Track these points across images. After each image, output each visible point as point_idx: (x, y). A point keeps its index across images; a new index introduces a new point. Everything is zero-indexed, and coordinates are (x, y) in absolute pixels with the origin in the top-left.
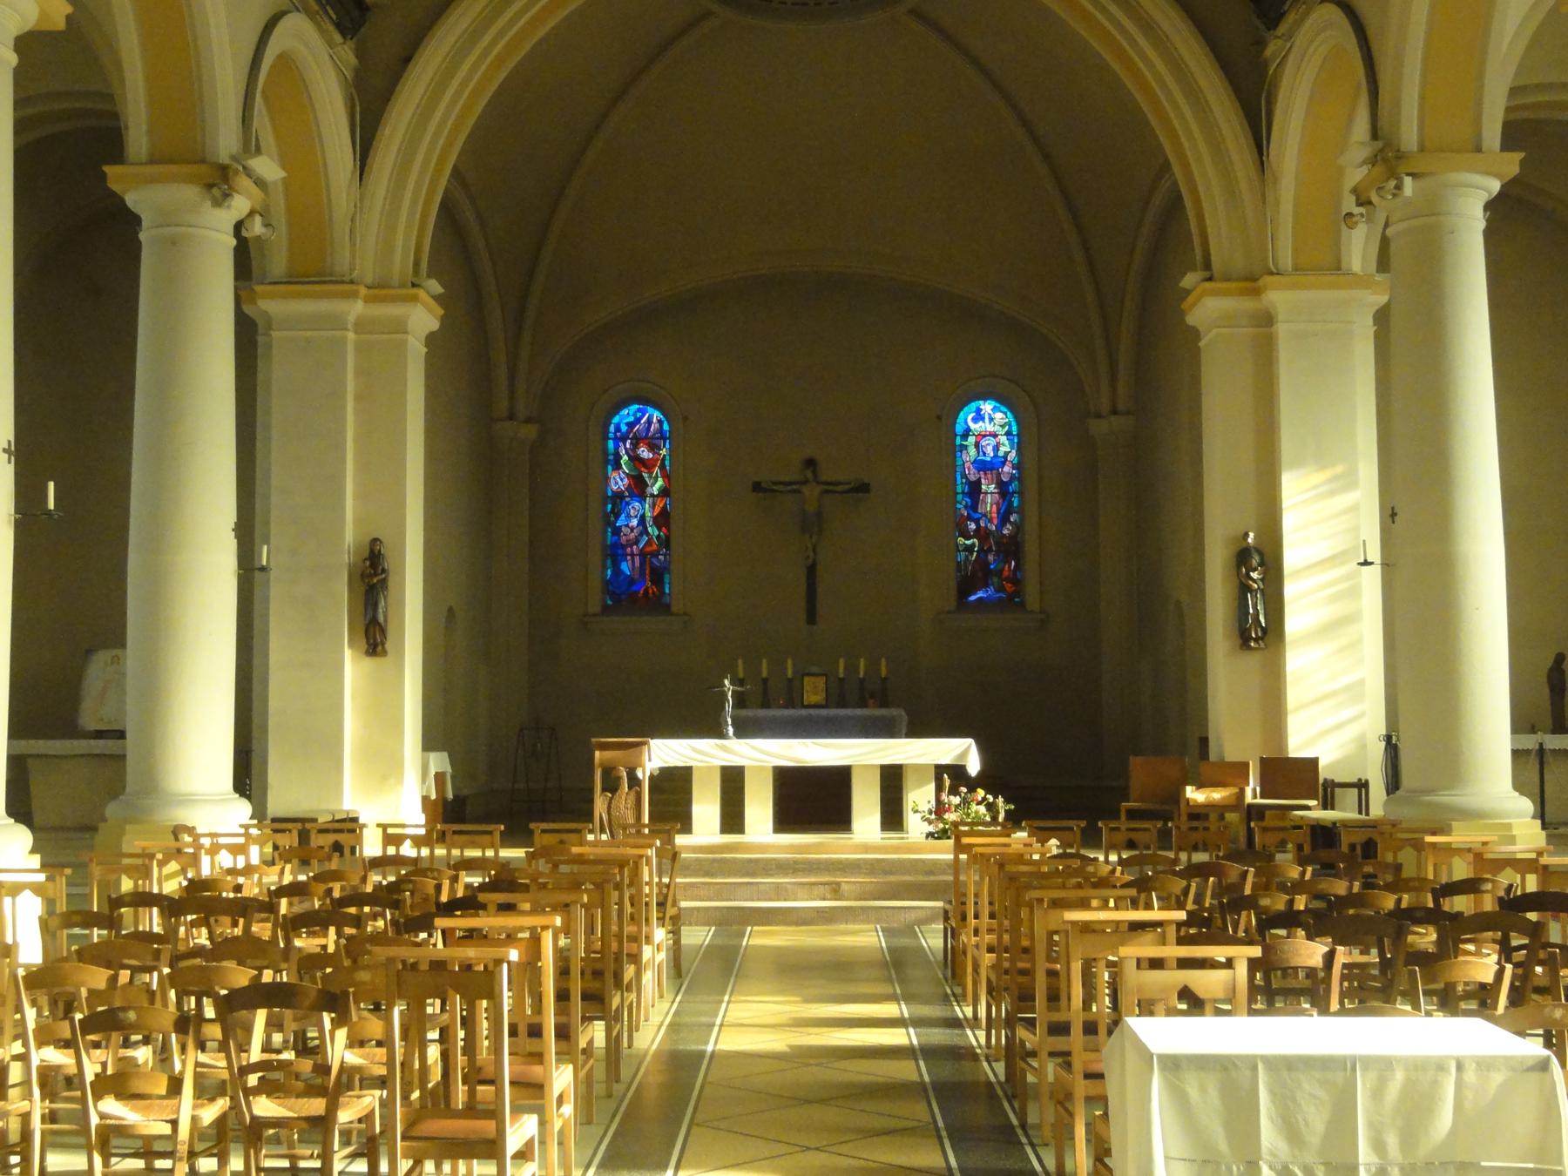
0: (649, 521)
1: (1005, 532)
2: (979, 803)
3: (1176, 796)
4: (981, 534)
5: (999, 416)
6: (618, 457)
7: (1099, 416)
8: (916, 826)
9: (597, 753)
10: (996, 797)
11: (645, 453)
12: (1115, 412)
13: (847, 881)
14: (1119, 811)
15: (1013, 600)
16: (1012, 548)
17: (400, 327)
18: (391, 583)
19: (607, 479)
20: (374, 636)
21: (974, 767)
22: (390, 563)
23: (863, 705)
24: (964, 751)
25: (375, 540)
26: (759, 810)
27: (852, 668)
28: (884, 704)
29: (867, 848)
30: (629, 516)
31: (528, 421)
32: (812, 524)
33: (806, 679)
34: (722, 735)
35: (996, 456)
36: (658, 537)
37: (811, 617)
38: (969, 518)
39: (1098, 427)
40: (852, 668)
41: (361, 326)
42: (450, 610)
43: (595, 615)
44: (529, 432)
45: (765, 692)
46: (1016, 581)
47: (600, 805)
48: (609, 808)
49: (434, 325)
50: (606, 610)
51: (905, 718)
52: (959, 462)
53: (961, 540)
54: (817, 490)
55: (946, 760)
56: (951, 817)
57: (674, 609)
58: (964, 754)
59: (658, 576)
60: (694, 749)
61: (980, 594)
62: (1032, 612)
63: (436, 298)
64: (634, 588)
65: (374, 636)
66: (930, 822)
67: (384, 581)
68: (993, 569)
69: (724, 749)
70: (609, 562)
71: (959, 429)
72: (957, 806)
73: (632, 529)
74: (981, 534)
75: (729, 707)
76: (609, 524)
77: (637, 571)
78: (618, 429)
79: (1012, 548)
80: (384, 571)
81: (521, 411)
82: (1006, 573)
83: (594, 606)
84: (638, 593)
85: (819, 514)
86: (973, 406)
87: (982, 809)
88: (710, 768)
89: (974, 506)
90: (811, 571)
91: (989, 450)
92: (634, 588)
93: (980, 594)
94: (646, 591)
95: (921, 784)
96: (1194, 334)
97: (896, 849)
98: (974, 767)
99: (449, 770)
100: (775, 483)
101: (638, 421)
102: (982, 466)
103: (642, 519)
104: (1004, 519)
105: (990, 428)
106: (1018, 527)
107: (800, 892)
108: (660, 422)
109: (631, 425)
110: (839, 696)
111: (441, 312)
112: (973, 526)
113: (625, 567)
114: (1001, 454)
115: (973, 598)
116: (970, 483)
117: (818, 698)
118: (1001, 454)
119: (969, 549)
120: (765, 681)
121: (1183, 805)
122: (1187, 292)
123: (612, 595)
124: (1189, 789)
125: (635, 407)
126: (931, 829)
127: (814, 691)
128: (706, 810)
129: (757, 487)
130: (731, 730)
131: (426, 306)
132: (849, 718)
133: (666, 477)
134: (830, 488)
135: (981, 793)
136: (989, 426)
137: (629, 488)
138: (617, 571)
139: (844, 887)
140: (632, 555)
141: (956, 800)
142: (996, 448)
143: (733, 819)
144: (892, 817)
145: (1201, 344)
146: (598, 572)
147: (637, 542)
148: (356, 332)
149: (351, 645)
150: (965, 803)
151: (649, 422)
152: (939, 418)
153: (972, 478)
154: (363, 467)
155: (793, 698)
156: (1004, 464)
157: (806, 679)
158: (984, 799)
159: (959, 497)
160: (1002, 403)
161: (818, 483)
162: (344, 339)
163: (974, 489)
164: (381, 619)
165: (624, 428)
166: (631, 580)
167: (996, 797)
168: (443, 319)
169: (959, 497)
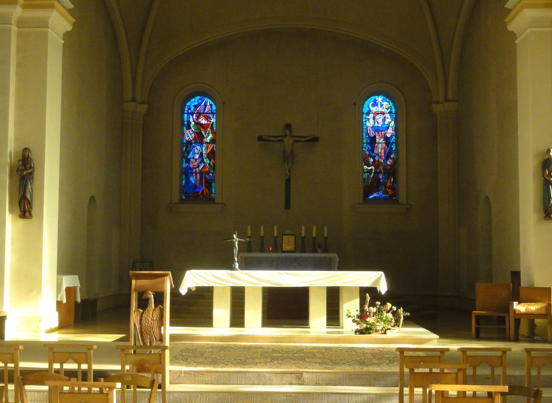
0: (205, 155)
1: (388, 163)
2: (388, 312)
3: (507, 308)
4: (376, 164)
5: (385, 103)
6: (189, 123)
7: (438, 102)
8: (348, 325)
9: (134, 282)
10: (398, 308)
11: (203, 121)
12: (446, 100)
13: (309, 370)
14: (470, 314)
15: (392, 198)
16: (392, 172)
17: (44, 24)
18: (36, 175)
19: (183, 134)
20: (25, 207)
21: (383, 288)
22: (36, 164)
23: (315, 251)
24: (377, 279)
25: (26, 149)
26: (254, 312)
27: (309, 231)
28: (325, 251)
29: (318, 339)
30: (194, 153)
31: (142, 103)
32: (289, 158)
33: (284, 237)
34: (232, 268)
35: (384, 124)
36: (209, 164)
37: (288, 206)
38: (370, 156)
39: (438, 108)
40: (309, 231)
41: (21, 23)
42: (92, 197)
43: (175, 204)
44: (143, 109)
45: (262, 244)
46: (393, 188)
47: (134, 318)
48: (141, 320)
49: (69, 28)
50: (182, 201)
51: (337, 259)
52: (365, 127)
53: (365, 167)
54: (291, 140)
55: (367, 284)
56: (371, 320)
57: (217, 201)
58: (378, 281)
59: (209, 184)
60: (215, 277)
61: (375, 195)
62: (402, 204)
63: (70, 11)
64: (196, 190)
65: (25, 207)
66: (358, 324)
67: (31, 174)
68: (383, 182)
69: (233, 276)
70: (184, 177)
71: (365, 110)
72: (375, 314)
73: (196, 160)
74: (376, 164)
75: (236, 251)
76: (183, 157)
77: (198, 182)
78: (189, 109)
79: (392, 172)
80: (31, 167)
81: (139, 98)
82: (388, 184)
83: (176, 199)
84: (198, 193)
85: (292, 152)
86: (372, 98)
87: (390, 315)
88: (224, 288)
89: (372, 150)
90: (288, 182)
91: (380, 121)
92: (196, 190)
93: (375, 195)
94: (203, 191)
95: (351, 299)
96: (513, 36)
97: (337, 341)
98: (383, 288)
99: (79, 285)
100: (269, 136)
101: (199, 104)
102: (377, 130)
103: (201, 155)
104: (388, 157)
105: (379, 109)
106: (395, 161)
107: (274, 378)
108: (211, 105)
109: (196, 107)
110: (301, 247)
111: (73, 20)
112: (372, 160)
113: (192, 179)
114: (386, 123)
115: (371, 197)
116: (370, 138)
117: (291, 247)
118: (386, 123)
119: (370, 172)
120: (262, 238)
121: (511, 313)
122: (509, 11)
123: (185, 193)
124: (515, 303)
125: (198, 98)
126: (358, 327)
127: (288, 243)
128: (221, 312)
129: (260, 138)
130: (237, 265)
131: (59, 11)
132: (306, 259)
133: (214, 133)
134: (298, 140)
135: (389, 305)
136: (379, 114)
137: (194, 138)
138: (188, 181)
139: (305, 376)
140: (196, 173)
141: (374, 310)
142: (384, 120)
143: (237, 319)
144: (333, 316)
145: (517, 41)
146: (177, 181)
147: (198, 167)
148: (18, 27)
149: (11, 211)
150: (379, 311)
151: (206, 105)
152: (355, 104)
153: (372, 135)
154: (20, 106)
155: (277, 248)
156: (388, 128)
157: (284, 237)
158: (391, 309)
159: (365, 145)
160: (387, 97)
161: (292, 136)
162: (10, 29)
163: (373, 140)
164: (28, 196)
165: (192, 108)
166: (195, 186)
167: (398, 308)
168: (74, 25)
169: (365, 145)
